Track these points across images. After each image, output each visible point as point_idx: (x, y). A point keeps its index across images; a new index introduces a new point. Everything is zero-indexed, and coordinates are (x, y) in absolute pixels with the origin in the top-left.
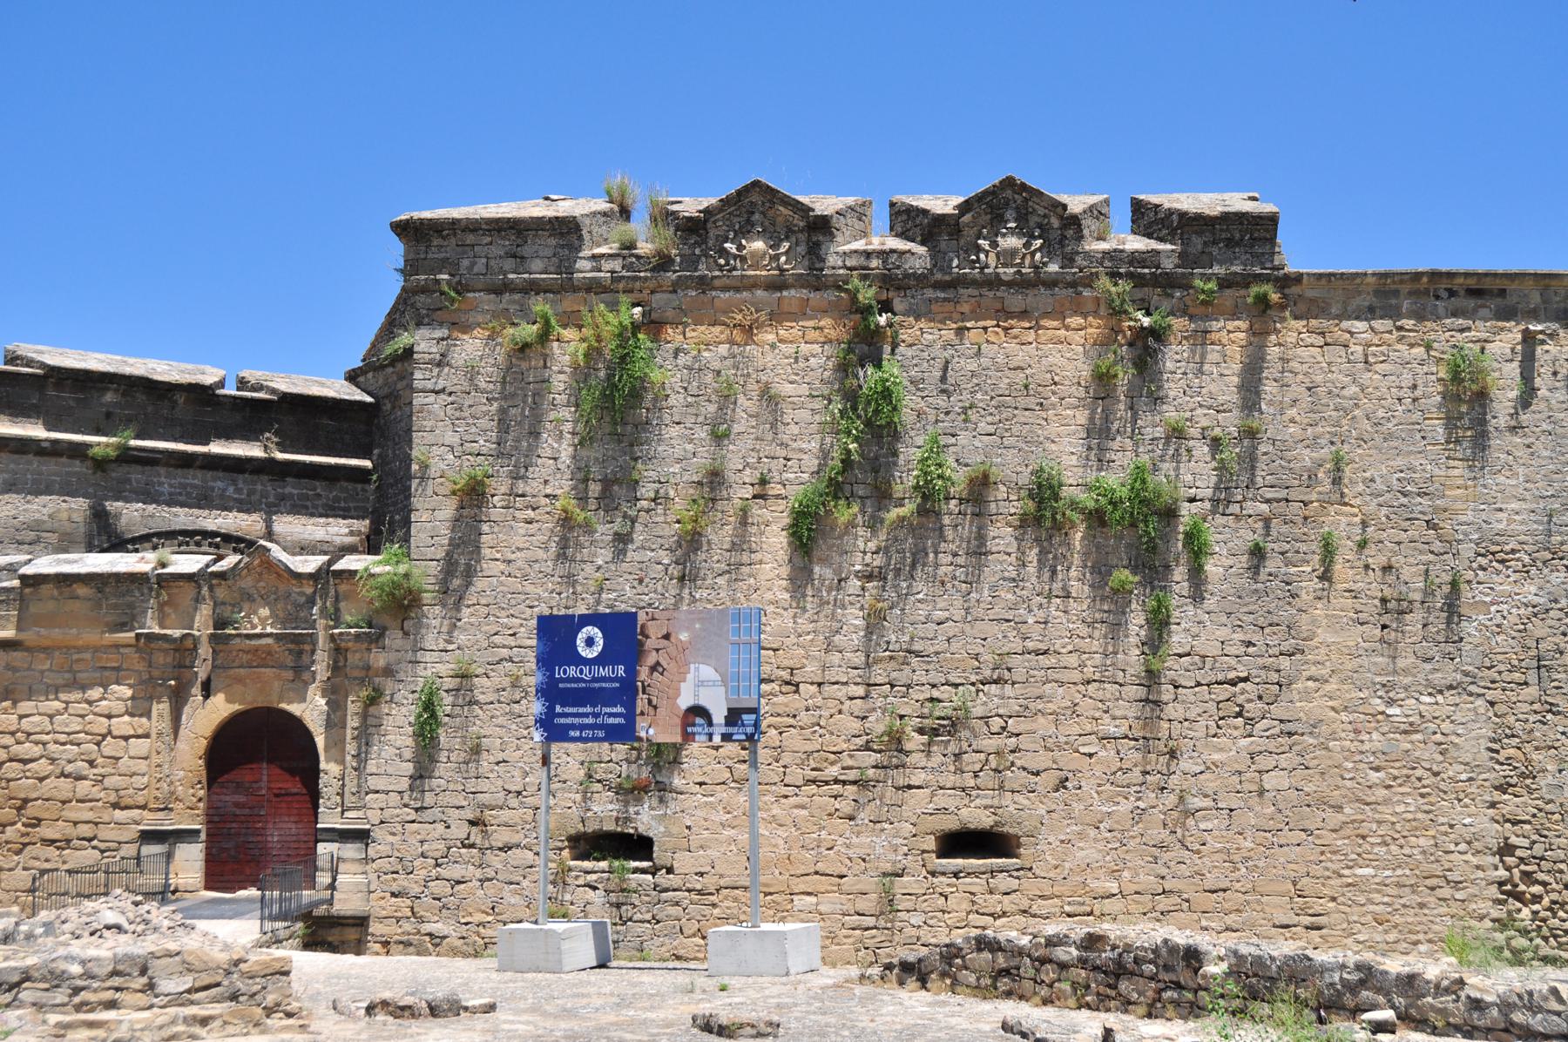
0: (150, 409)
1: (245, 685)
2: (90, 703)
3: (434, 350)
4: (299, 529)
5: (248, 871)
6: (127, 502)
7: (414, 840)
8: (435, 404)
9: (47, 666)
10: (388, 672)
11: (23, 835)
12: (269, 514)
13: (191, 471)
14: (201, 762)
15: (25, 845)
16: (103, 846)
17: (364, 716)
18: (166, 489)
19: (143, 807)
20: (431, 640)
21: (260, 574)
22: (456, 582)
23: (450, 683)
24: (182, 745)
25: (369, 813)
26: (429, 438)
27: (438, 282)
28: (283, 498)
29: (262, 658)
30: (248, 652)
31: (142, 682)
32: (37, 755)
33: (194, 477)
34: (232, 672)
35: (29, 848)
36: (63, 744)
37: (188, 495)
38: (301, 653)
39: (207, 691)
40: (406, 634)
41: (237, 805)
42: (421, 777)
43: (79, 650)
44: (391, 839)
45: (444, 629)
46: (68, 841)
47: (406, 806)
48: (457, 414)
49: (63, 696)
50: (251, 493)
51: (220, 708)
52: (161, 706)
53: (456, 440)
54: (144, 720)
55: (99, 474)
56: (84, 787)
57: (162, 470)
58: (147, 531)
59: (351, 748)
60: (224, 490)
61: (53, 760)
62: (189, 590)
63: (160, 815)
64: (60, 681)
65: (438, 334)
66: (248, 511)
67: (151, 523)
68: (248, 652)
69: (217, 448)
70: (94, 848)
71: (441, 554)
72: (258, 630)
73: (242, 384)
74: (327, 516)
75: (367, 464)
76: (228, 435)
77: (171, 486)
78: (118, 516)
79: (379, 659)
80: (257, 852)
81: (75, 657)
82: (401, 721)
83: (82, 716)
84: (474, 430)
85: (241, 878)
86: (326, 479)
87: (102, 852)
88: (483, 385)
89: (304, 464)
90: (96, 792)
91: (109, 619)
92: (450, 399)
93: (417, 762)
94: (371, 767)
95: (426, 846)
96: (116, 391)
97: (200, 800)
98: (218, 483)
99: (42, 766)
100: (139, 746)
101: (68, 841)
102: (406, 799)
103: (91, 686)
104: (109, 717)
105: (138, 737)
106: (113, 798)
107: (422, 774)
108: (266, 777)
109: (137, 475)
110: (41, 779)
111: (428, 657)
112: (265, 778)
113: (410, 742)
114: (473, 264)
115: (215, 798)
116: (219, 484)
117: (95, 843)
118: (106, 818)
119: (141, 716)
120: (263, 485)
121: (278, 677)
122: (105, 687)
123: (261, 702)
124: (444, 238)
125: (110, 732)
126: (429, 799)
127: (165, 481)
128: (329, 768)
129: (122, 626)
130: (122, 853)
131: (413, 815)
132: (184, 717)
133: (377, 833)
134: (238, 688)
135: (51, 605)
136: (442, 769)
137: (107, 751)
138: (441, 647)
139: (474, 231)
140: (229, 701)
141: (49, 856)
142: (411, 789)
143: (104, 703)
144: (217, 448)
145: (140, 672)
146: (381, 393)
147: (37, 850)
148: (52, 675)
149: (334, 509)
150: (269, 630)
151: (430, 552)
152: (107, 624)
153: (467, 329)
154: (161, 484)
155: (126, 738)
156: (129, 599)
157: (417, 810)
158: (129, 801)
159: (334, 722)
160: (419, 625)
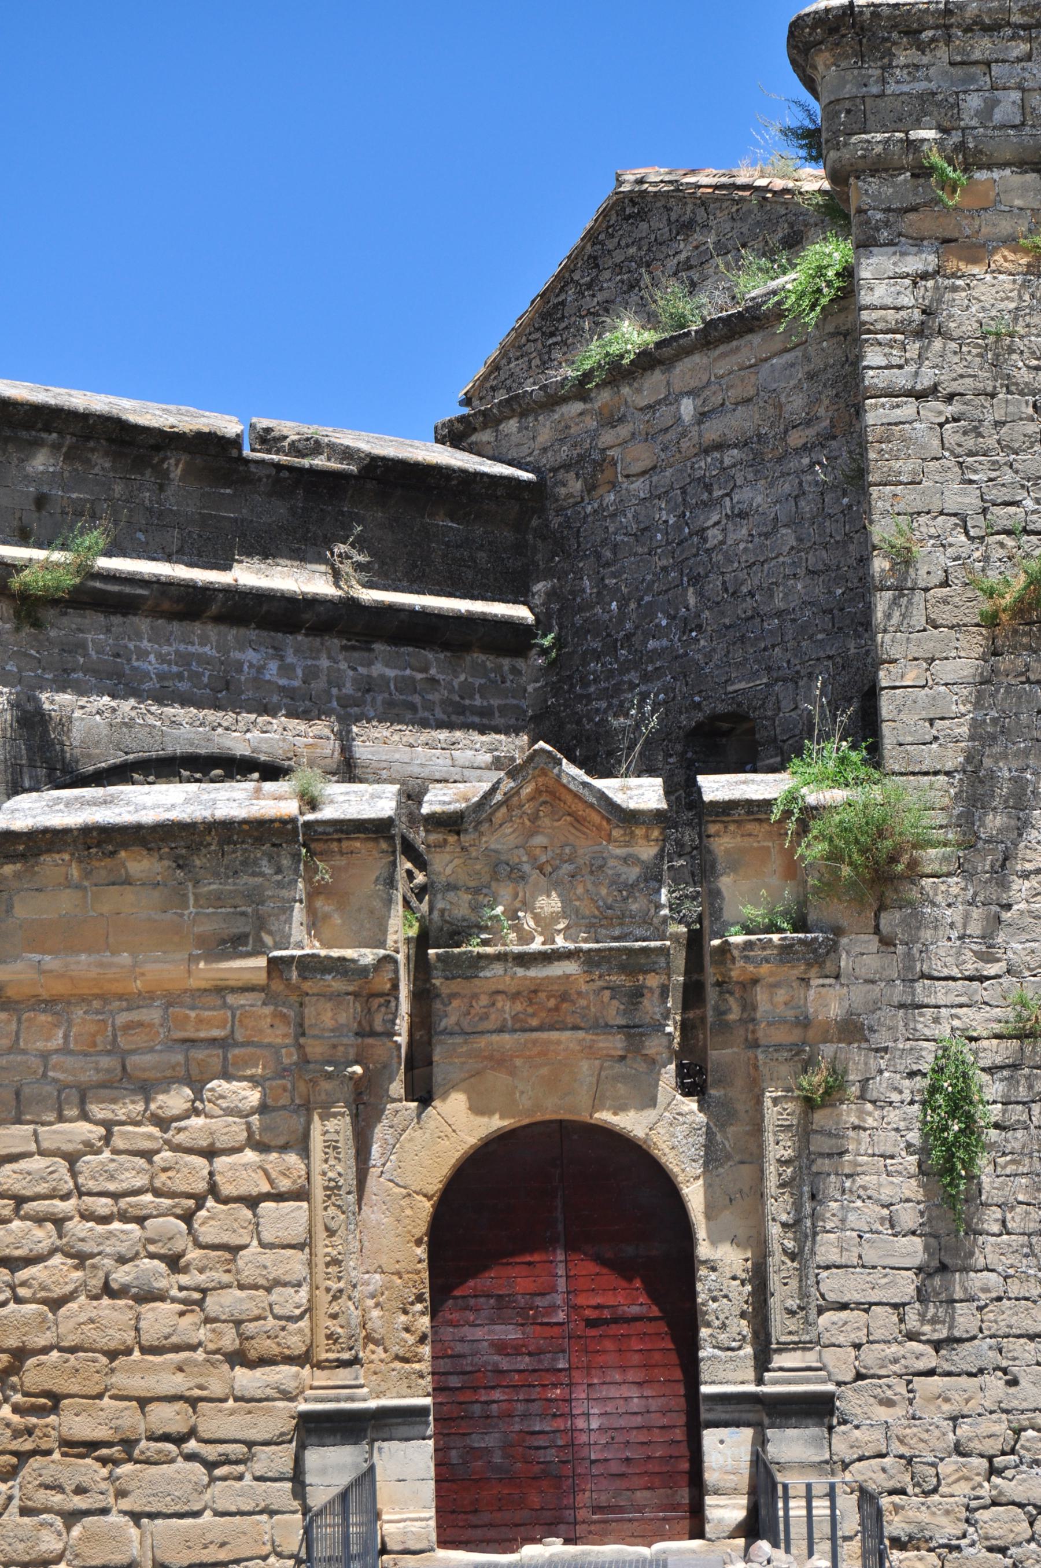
0: (118, 489)
1: (512, 1072)
2: (163, 1123)
3: (907, 300)
4: (402, 754)
5: (535, 1499)
6: (81, 692)
7: (935, 1415)
8: (920, 420)
9: (58, 1041)
10: (852, 1030)
11: (17, 1434)
12: (346, 720)
13: (197, 628)
14: (421, 1252)
15: (23, 1457)
16: (211, 1452)
17: (804, 1133)
18: (151, 665)
19: (302, 1360)
20: (944, 955)
21: (535, 818)
22: (994, 822)
23: (996, 1052)
24: (373, 1214)
25: (829, 1355)
26: (910, 498)
27: (911, 145)
28: (368, 686)
29: (553, 1009)
30: (515, 996)
31: (282, 1072)
32: (44, 1247)
33: (204, 641)
34: (482, 1042)
35: (36, 1462)
36: (105, 1220)
37: (195, 676)
38: (636, 995)
39: (423, 1094)
40: (887, 942)
41: (501, 1347)
42: (943, 1268)
43: (133, 1001)
44: (883, 1413)
45: (975, 929)
46: (128, 1444)
47: (912, 1336)
48: (970, 442)
49: (98, 1111)
50: (311, 674)
51: (455, 1127)
52: (332, 1125)
53: (968, 500)
54: (292, 1159)
55: (27, 630)
56: (159, 1319)
57: (143, 624)
58: (120, 758)
59: (779, 1208)
60: (261, 669)
61: (81, 1259)
62: (369, 859)
63: (343, 1376)
64: (89, 1076)
65: (914, 264)
66: (306, 715)
67: (129, 742)
68: (515, 996)
69: (247, 575)
70: (190, 1457)
71: (954, 759)
72: (537, 945)
73: (266, 439)
74: (451, 727)
75: (521, 612)
76: (266, 548)
77: (162, 658)
78: (65, 723)
79: (829, 1003)
80: (551, 1455)
81: (122, 1018)
82: (888, 1142)
83: (148, 1155)
84: (1008, 476)
85: (524, 1515)
86: (445, 646)
87: (210, 1466)
88: (1024, 376)
89: (410, 612)
90: (189, 1329)
91: (206, 927)
92: (950, 410)
93: (930, 1233)
94: (827, 1248)
95: (964, 1430)
96: (55, 447)
97: (422, 1340)
98: (251, 654)
99: (57, 1273)
100: (285, 1219)
101: (128, 1444)
102: (913, 1321)
103: (165, 1084)
104: (210, 1153)
105: (279, 1197)
106: (229, 1340)
107: (944, 1262)
108: (562, 1283)
109: (96, 634)
110: (56, 1304)
111: (941, 993)
112: (561, 1284)
113: (912, 1188)
114: (991, 105)
115: (447, 1333)
116: (250, 656)
117: (192, 1445)
118: (216, 1388)
119: (283, 1149)
120: (333, 661)
121: (590, 1051)
122: (198, 1087)
123: (552, 1109)
124: (921, 48)
125: (213, 1189)
126: (965, 1319)
127: (152, 646)
128: (721, 1262)
129: (235, 944)
130: (259, 1467)
131: (930, 1360)
132: (376, 1150)
133: (850, 1402)
134: (499, 1079)
135: (66, 902)
136: (990, 1250)
137: (208, 1233)
138: (970, 968)
139: (991, 29)
140: (477, 1108)
141: (86, 1481)
142: (922, 1296)
143: (196, 1122)
144: (247, 575)
145: (275, 1049)
146: (548, 460)
147: (55, 1466)
148: (69, 1061)
149: (461, 710)
150: (560, 942)
151: (929, 756)
152: (201, 941)
153: (977, 251)
154: (143, 654)
155: (252, 1202)
156: (246, 880)
157: (937, 1345)
158: (269, 1347)
159: (731, 1149)
160: (916, 922)
